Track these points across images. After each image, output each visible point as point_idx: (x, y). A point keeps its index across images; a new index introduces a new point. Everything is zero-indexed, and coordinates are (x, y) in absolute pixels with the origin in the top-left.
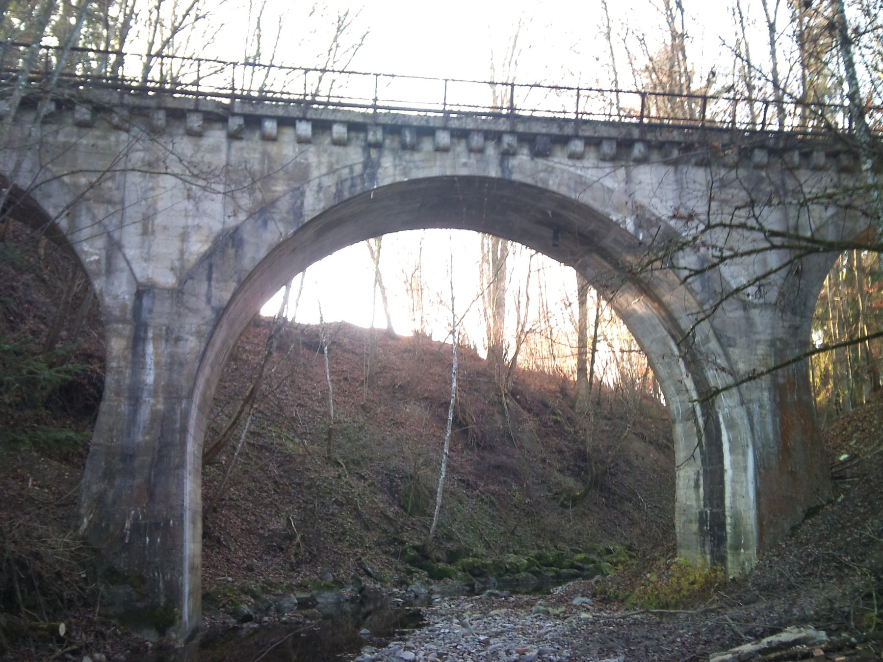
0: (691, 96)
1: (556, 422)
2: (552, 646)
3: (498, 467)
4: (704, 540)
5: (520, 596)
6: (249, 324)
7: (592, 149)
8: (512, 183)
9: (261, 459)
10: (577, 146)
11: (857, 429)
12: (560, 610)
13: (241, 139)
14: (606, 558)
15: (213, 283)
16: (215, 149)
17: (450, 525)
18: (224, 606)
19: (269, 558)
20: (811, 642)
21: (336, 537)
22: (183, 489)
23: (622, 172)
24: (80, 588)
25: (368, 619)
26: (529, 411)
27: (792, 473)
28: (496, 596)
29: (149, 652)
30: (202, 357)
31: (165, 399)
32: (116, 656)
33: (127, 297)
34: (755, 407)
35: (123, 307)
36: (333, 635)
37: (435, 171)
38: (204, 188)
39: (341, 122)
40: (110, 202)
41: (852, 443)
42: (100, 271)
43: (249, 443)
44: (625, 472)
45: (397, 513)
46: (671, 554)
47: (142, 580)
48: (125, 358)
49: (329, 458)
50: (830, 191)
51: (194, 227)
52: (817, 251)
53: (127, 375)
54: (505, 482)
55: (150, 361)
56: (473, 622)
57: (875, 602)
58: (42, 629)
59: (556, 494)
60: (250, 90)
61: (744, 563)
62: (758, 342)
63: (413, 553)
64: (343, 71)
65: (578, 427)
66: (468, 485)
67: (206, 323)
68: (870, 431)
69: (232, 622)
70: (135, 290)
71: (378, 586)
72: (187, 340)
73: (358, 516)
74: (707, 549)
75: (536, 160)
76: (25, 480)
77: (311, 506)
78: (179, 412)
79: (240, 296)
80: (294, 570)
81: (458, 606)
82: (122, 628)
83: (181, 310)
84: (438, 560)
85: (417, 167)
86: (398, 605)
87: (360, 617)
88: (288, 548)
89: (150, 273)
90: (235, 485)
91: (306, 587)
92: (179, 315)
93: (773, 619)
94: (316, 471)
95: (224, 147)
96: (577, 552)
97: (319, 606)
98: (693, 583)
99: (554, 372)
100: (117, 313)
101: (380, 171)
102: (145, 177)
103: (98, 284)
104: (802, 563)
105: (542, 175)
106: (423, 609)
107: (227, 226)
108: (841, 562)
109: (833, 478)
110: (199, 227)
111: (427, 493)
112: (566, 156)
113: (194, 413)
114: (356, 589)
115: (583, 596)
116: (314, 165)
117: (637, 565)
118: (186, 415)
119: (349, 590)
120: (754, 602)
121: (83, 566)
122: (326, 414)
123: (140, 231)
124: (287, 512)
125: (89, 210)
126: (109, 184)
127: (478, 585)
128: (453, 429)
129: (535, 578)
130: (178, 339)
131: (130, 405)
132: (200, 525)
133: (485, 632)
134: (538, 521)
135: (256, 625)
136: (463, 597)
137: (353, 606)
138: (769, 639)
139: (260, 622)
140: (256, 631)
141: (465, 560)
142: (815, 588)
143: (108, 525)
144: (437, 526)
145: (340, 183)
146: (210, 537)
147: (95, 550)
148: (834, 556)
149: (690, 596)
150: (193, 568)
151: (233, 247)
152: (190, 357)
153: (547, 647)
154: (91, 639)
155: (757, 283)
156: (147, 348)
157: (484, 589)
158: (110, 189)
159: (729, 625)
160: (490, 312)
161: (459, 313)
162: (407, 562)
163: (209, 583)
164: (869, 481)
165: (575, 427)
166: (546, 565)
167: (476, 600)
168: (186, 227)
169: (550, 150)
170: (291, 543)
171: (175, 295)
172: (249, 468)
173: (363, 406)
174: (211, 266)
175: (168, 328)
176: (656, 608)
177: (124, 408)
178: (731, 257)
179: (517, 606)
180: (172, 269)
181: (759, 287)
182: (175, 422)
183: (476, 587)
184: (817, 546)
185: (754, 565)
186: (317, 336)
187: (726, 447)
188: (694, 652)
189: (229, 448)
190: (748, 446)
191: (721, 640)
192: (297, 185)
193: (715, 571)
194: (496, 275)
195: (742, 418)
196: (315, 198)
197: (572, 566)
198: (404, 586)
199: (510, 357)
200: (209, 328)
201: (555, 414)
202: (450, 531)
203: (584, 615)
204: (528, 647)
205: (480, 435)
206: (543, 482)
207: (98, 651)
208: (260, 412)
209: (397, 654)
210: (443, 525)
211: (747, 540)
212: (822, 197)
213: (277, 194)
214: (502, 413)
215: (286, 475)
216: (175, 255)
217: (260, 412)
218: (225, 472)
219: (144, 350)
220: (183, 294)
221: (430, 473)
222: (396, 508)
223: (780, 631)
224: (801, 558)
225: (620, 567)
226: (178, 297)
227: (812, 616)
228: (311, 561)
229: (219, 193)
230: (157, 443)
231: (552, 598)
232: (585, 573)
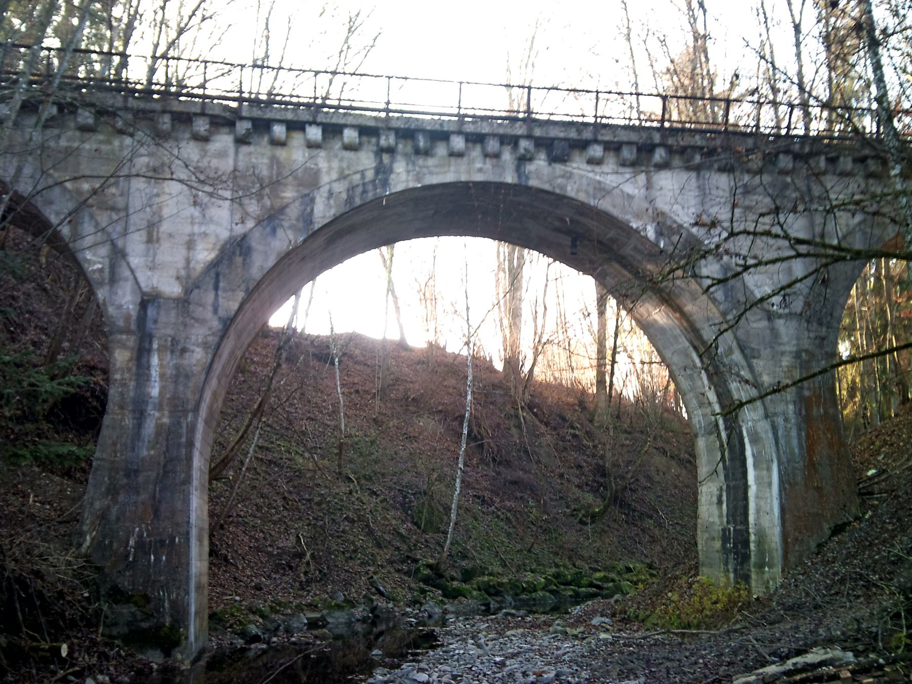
0: (714, 99)
1: (575, 436)
2: (570, 667)
3: (515, 483)
4: (727, 558)
5: (537, 616)
6: (257, 335)
7: (612, 154)
8: (529, 189)
10: (596, 151)
11: (885, 443)
12: (578, 630)
13: (249, 143)
14: (626, 576)
15: (220, 293)
16: (222, 154)
17: (465, 543)
18: (231, 626)
19: (277, 576)
20: (837, 663)
21: (347, 555)
23: (642, 178)
24: (82, 607)
25: (380, 639)
26: (547, 424)
27: (819, 489)
28: (513, 615)
29: (154, 674)
30: (209, 369)
31: (170, 412)
32: (120, 678)
33: (131, 307)
34: (780, 420)
35: (128, 318)
36: (344, 656)
37: (450, 178)
38: (211, 195)
39: (352, 126)
40: (113, 209)
41: (880, 458)
42: (103, 280)
43: (257, 458)
44: (645, 488)
46: (693, 572)
47: (147, 599)
49: (340, 473)
50: (857, 197)
52: (844, 259)
53: (131, 387)
54: (521, 498)
55: (155, 373)
57: (904, 622)
58: (43, 650)
59: (575, 510)
61: (768, 582)
62: (783, 353)
63: (427, 572)
64: (354, 74)
65: (596, 442)
67: (213, 334)
68: (899, 445)
69: (240, 642)
71: (390, 605)
72: (193, 352)
73: (371, 533)
74: (731, 567)
75: (554, 165)
76: (25, 496)
77: (321, 523)
78: (184, 426)
79: (248, 306)
80: (303, 589)
81: (473, 626)
82: (126, 648)
83: (187, 320)
84: (453, 579)
85: (431, 173)
86: (411, 625)
88: (298, 566)
90: (243, 501)
91: (316, 606)
92: (185, 325)
93: (798, 640)
94: (326, 487)
95: (231, 151)
96: (596, 570)
97: (329, 626)
98: (716, 603)
99: (572, 384)
100: (121, 323)
101: (393, 176)
102: (149, 183)
103: (101, 294)
104: (828, 582)
105: (560, 181)
106: (437, 629)
107: (234, 234)
108: (869, 581)
109: (860, 494)
110: (205, 234)
111: (441, 510)
112: (585, 161)
113: (200, 426)
116: (324, 170)
117: (658, 584)
118: (192, 429)
119: (361, 609)
120: (779, 622)
121: (86, 584)
122: (337, 428)
123: (144, 238)
124: (296, 529)
125: (92, 217)
126: (113, 190)
128: (467, 444)
129: (553, 597)
130: (184, 350)
131: (134, 418)
132: (206, 542)
134: (556, 538)
135: (264, 646)
136: (478, 617)
138: (794, 660)
139: (268, 643)
140: (264, 652)
142: (842, 607)
143: (111, 543)
144: (451, 544)
145: (352, 189)
146: (217, 556)
147: (97, 568)
148: (861, 575)
149: (712, 616)
150: (199, 587)
152: (196, 369)
153: (565, 669)
154: (94, 660)
155: (782, 292)
156: (152, 360)
157: (500, 609)
158: (114, 195)
159: (753, 646)
160: (506, 322)
161: (474, 323)
163: (216, 602)
164: (897, 497)
165: (593, 441)
167: (492, 620)
168: (192, 235)
169: (568, 155)
171: (180, 305)
172: (257, 483)
173: (374, 420)
174: (218, 275)
175: (173, 339)
176: (677, 628)
177: (129, 422)
178: (755, 266)
179: (534, 626)
180: (178, 278)
181: (784, 296)
182: (181, 437)
183: (492, 606)
184: (844, 564)
185: (779, 584)
186: (328, 347)
187: (750, 461)
188: (717, 674)
190: (772, 461)
191: (745, 662)
192: (306, 192)
193: (738, 590)
194: (512, 284)
195: (766, 432)
197: (591, 585)
198: (417, 606)
199: (526, 369)
200: (217, 339)
201: (573, 428)
203: (603, 636)
204: (546, 668)
207: (101, 672)
208: (268, 426)
209: (411, 676)
211: (771, 558)
212: (849, 203)
213: (286, 201)
214: (519, 426)
215: (296, 490)
216: (181, 264)
217: (268, 426)
219: (148, 362)
221: (444, 489)
222: (409, 525)
223: (806, 652)
224: (827, 577)
225: (641, 586)
227: (838, 637)
228: (321, 579)
229: (227, 199)
230: (162, 458)
231: (570, 618)
232: (605, 592)
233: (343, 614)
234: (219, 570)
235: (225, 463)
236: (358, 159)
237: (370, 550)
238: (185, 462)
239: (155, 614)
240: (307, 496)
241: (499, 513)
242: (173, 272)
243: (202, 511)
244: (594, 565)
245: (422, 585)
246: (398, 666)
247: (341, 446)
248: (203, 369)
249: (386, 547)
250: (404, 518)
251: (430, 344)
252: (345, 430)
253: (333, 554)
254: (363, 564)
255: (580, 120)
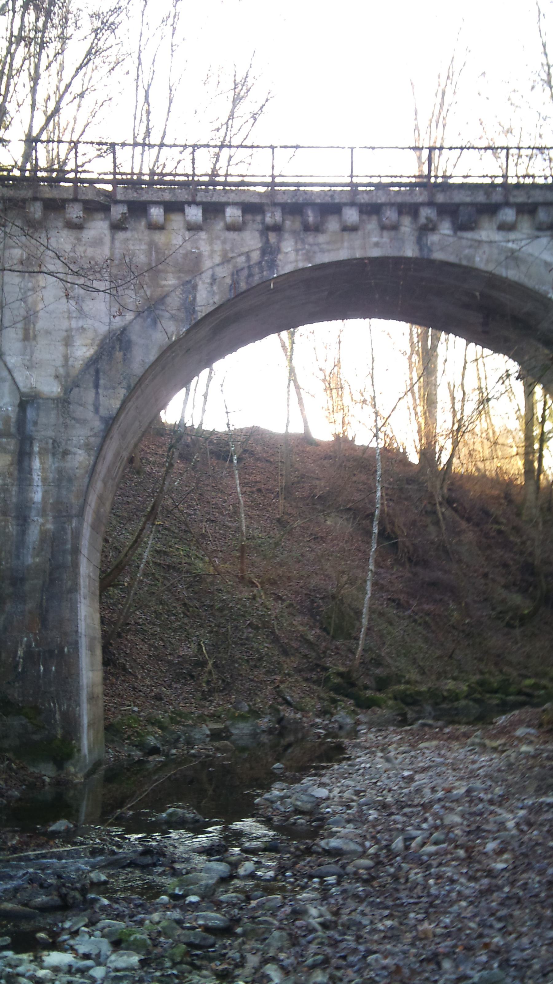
1: (500, 532)
2: (483, 782)
3: (433, 584)
5: (457, 726)
7: (526, 217)
8: (432, 262)
9: (169, 580)
10: (509, 215)
12: (499, 742)
13: (125, 229)
15: (100, 391)
16: (97, 242)
17: (379, 649)
18: (129, 738)
19: (179, 686)
22: (76, 614)
25: (290, 750)
26: (469, 520)
28: (430, 726)
29: (47, 788)
30: (92, 472)
31: (54, 517)
32: (10, 792)
36: (252, 768)
37: (343, 255)
39: (235, 204)
43: (155, 563)
45: (318, 637)
48: (11, 475)
49: (243, 578)
51: (78, 329)
53: (14, 493)
54: (441, 600)
55: (37, 477)
56: (398, 756)
59: (501, 612)
60: (141, 174)
63: (337, 680)
65: (524, 538)
66: (399, 605)
67: (95, 435)
69: (137, 754)
70: (17, 402)
71: (299, 716)
72: (75, 454)
73: (276, 640)
75: (459, 234)
77: (224, 630)
78: (69, 532)
79: (130, 404)
80: (205, 699)
81: (385, 738)
82: (18, 761)
83: (68, 421)
84: (366, 688)
85: (322, 251)
86: (319, 737)
87: (280, 749)
88: (199, 675)
89: (33, 381)
90: (141, 608)
91: (219, 717)
92: (66, 426)
94: (228, 592)
95: (107, 239)
96: (525, 677)
99: (497, 474)
101: (280, 257)
102: (23, 277)
105: (467, 251)
106: (346, 741)
110: (83, 329)
111: (352, 614)
112: (495, 227)
113: (86, 531)
114: (274, 719)
115: (528, 726)
116: (206, 254)
118: (77, 535)
119: (266, 720)
122: (239, 529)
123: (21, 336)
124: (197, 636)
127: (410, 715)
128: (378, 543)
129: (477, 706)
130: (66, 453)
131: (18, 525)
132: (99, 652)
133: (410, 767)
134: (480, 643)
135: (162, 758)
136: (392, 728)
137: (271, 737)
139: (167, 755)
140: (164, 765)
141: (396, 687)
144: (364, 650)
145: (237, 272)
146: (115, 665)
150: (92, 698)
151: (120, 349)
152: (79, 472)
153: (478, 784)
157: (417, 719)
160: (420, 409)
162: (331, 690)
163: (114, 713)
165: (521, 536)
166: (488, 692)
167: (406, 731)
168: (69, 330)
169: (475, 222)
170: (202, 670)
173: (279, 520)
174: (97, 372)
175: (54, 441)
179: (452, 737)
180: (57, 377)
183: (409, 716)
189: (133, 568)
192: (187, 279)
196: (209, 292)
197: (520, 693)
198: (328, 716)
200: (98, 440)
201: (497, 523)
202: (379, 656)
203: (524, 748)
204: (457, 784)
205: (411, 548)
206: (486, 600)
209: (310, 790)
210: (370, 649)
214: (437, 523)
215: (196, 596)
216: (59, 362)
218: (129, 593)
220: (69, 403)
221: (355, 592)
222: (318, 631)
226: (63, 407)
228: (224, 689)
229: (99, 291)
230: (48, 566)
231: (493, 729)
232: (536, 700)
233: (248, 724)
234: (117, 679)
235: (119, 568)
236: (242, 239)
237: (276, 658)
238: (71, 569)
239: (46, 726)
240: (208, 602)
241: (417, 617)
242: (51, 371)
243: (93, 619)
244: (524, 672)
245: (332, 694)
246: (299, 780)
247: (242, 549)
248: (87, 472)
249: (293, 655)
250: (311, 624)
251: (337, 437)
252: (247, 533)
253: (236, 662)
254: (269, 672)
255: (529, 181)
